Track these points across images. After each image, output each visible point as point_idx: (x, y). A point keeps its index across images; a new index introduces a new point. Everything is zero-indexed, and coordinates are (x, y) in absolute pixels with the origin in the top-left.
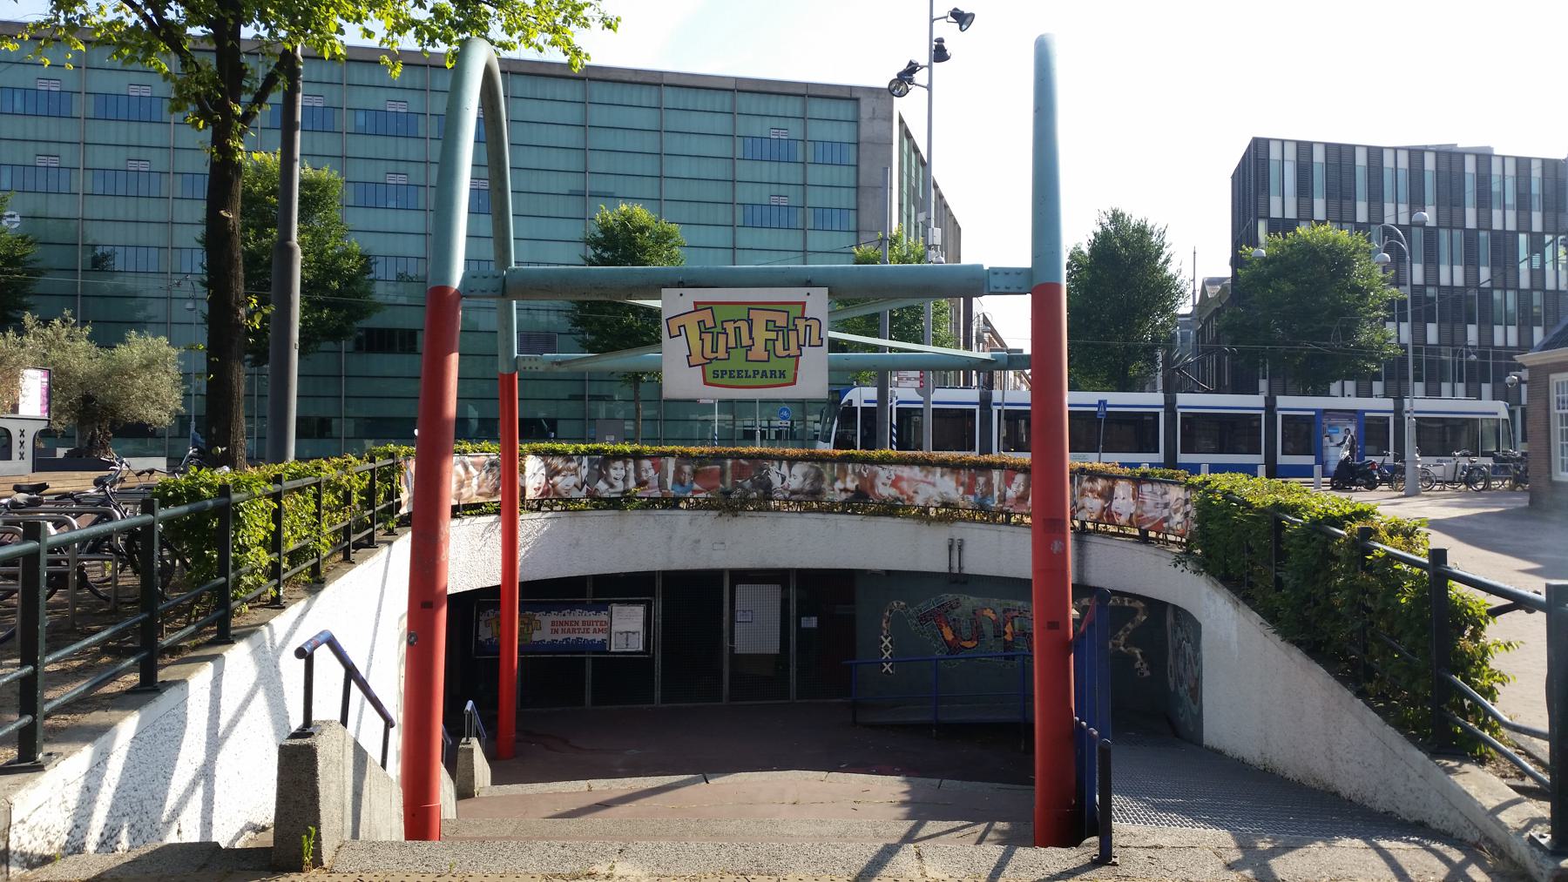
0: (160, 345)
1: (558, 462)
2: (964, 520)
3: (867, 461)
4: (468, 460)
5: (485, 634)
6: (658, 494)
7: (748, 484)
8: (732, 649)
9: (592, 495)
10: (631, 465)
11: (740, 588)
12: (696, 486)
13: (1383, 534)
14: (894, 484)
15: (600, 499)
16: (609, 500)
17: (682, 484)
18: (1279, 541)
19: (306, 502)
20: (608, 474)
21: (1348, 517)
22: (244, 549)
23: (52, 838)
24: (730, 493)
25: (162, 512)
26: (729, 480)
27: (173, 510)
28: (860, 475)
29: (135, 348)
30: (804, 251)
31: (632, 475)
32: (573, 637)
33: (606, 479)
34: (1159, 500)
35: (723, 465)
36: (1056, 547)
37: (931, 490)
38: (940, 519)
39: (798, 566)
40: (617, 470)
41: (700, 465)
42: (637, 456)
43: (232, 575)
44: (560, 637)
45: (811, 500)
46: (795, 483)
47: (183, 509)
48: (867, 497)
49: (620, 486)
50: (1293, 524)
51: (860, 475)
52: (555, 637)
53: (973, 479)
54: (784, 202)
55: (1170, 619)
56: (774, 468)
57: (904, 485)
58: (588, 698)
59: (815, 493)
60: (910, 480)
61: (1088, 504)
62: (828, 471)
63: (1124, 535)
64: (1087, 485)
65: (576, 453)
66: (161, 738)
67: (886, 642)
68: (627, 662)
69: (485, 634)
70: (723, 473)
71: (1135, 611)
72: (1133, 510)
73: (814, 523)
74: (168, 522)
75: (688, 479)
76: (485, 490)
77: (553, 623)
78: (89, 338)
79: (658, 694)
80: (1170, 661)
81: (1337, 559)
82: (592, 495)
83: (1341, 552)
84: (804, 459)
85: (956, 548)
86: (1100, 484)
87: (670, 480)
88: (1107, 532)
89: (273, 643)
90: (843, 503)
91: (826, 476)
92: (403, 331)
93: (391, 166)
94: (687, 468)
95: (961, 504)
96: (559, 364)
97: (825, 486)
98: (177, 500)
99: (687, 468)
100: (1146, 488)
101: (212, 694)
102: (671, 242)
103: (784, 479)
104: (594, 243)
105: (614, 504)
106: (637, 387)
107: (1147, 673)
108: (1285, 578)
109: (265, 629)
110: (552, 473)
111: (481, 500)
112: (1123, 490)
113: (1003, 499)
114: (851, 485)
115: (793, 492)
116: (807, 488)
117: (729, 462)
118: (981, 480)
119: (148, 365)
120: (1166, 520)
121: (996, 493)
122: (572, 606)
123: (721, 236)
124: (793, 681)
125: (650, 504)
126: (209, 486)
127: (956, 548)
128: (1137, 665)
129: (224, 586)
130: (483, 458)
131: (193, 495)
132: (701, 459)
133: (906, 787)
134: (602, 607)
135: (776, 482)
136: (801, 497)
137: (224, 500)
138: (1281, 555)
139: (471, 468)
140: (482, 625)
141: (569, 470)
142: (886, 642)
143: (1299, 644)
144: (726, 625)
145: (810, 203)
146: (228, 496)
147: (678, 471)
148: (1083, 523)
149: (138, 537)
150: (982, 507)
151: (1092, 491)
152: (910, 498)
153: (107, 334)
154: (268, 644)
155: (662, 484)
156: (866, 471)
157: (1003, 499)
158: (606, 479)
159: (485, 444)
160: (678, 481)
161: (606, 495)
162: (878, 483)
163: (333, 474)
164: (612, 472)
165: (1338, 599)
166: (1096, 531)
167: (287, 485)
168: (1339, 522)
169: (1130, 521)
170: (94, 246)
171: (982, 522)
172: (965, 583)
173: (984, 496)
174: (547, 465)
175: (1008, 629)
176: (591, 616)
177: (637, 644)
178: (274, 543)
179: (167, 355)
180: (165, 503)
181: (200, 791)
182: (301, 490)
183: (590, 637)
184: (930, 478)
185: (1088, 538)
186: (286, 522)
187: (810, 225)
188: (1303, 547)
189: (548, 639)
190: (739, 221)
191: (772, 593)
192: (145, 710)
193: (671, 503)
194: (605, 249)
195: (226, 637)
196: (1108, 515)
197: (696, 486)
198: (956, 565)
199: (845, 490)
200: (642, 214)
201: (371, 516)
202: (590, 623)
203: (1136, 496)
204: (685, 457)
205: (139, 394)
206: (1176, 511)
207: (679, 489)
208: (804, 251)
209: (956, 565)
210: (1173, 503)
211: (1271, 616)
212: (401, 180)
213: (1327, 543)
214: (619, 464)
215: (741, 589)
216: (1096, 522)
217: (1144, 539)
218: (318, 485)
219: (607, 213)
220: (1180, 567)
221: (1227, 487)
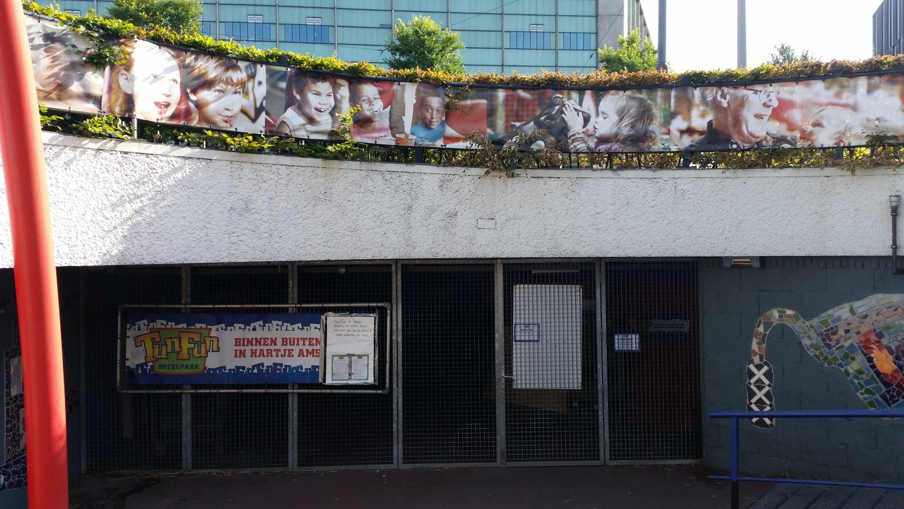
1: (209, 67)
6: (388, 139)
8: (509, 382)
11: (519, 290)
12: (450, 131)
14: (777, 115)
17: (427, 125)
20: (304, 99)
26: (500, 123)
28: (716, 106)
30: (556, 66)
32: (268, 362)
33: (301, 108)
35: (491, 99)
37: (848, 117)
38: (874, 163)
41: (457, 96)
44: (248, 362)
46: (605, 125)
49: (325, 123)
51: (716, 106)
52: (241, 362)
54: (540, 29)
56: (571, 101)
57: (796, 115)
58: (293, 454)
60: (806, 106)
67: (759, 374)
68: (350, 400)
70: (491, 112)
73: (636, 185)
75: (437, 119)
77: (238, 342)
79: (398, 449)
84: (620, 86)
91: (658, 112)
93: (251, 10)
94: (435, 102)
97: (655, 127)
102: (454, 45)
103: (587, 120)
104: (394, 49)
110: (195, 83)
115: (602, 140)
116: (625, 131)
122: (266, 316)
123: (493, 57)
124: (604, 433)
135: (575, 124)
140: (130, 342)
141: (229, 82)
142: (759, 374)
144: (499, 345)
145: (560, 29)
147: (421, 105)
152: (806, 136)
155: (395, 126)
156: (726, 97)
160: (422, 121)
161: (301, 134)
162: (748, 115)
164: (311, 97)
174: (183, 66)
176: (295, 331)
177: (365, 374)
183: (293, 362)
184: (847, 98)
187: (560, 46)
189: (231, 363)
190: (506, 45)
191: (569, 298)
193: (418, 155)
194: (402, 54)
197: (450, 131)
199: (690, 131)
200: (430, 23)
202: (293, 342)
207: (422, 133)
208: (556, 66)
212: (258, 20)
214: (324, 87)
219: (405, 25)
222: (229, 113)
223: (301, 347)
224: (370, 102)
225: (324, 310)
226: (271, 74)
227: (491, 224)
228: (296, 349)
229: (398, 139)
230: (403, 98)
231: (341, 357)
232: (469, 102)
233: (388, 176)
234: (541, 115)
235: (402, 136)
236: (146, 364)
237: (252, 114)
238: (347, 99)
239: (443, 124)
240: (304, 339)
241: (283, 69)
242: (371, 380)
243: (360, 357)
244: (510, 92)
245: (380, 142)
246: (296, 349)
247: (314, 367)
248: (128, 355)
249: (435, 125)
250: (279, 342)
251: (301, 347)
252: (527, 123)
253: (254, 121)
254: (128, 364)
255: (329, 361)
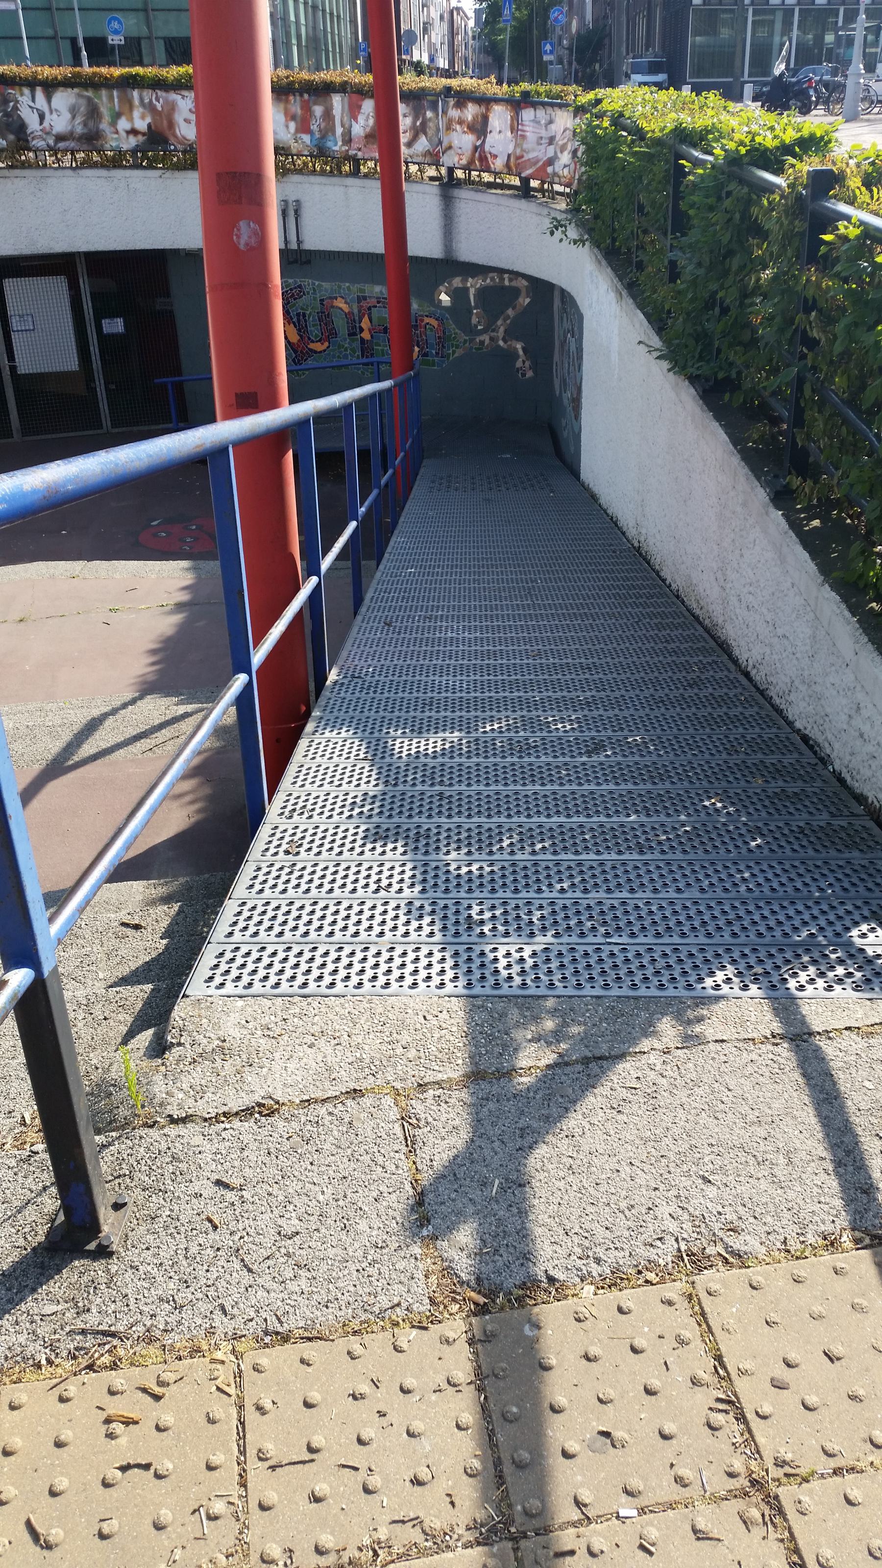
2: (300, 172)
3: (158, 84)
8: (13, 369)
13: (854, 183)
18: (677, 196)
21: (787, 149)
34: (544, 133)
36: (244, 233)
39: (84, 248)
45: (88, 148)
46: (60, 123)
48: (166, 141)
50: (703, 162)
51: (151, 108)
53: (307, 108)
55: (557, 303)
56: (24, 98)
59: (91, 139)
61: (456, 143)
62: (106, 101)
63: (502, 186)
64: (454, 113)
71: (516, 292)
72: (510, 149)
80: (556, 357)
81: (761, 233)
83: (771, 224)
85: (291, 213)
86: (471, 111)
88: (481, 183)
90: (134, 152)
91: (104, 110)
95: (295, 147)
97: (104, 126)
100: (528, 114)
103: (42, 117)
107: (530, 374)
108: (681, 263)
112: (499, 117)
113: (348, 139)
114: (141, 125)
115: (60, 138)
116: (79, 130)
118: (318, 110)
120: (550, 162)
121: (339, 130)
127: (291, 213)
128: (519, 364)
133: (188, 579)
136: (72, 144)
138: (680, 223)
143: (693, 380)
148: (451, 170)
150: (321, 152)
151: (461, 122)
156: (160, 99)
157: (348, 139)
165: (761, 310)
166: (468, 181)
168: (771, 159)
169: (507, 165)
171: (323, 173)
172: (308, 262)
173: (323, 137)
175: (365, 323)
185: (457, 192)
188: (711, 209)
191: (55, 288)
196: (480, 158)
198: (293, 237)
199: (133, 132)
203: (515, 127)
206: (563, 149)
209: (293, 237)
210: (553, 134)
211: (658, 320)
213: (749, 203)
216: (467, 168)
217: (525, 192)
220: (558, 234)
221: (617, 106)
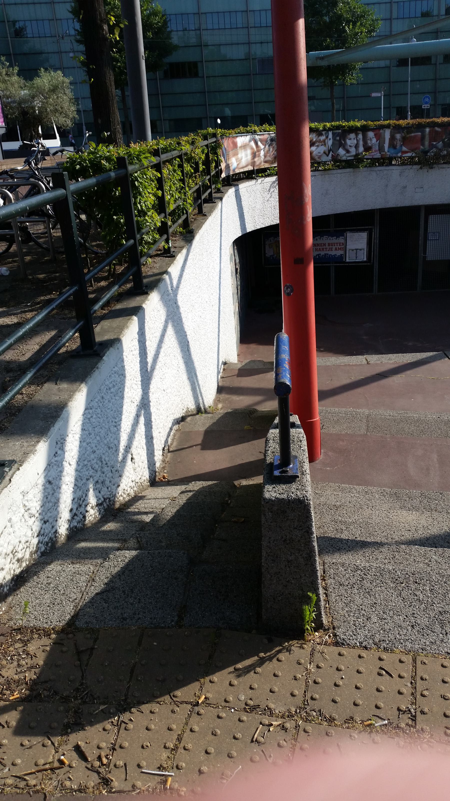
0: (59, 76)
4: (257, 137)
5: (269, 252)
6: (378, 155)
7: (440, 144)
8: (425, 258)
9: (335, 159)
10: (360, 136)
12: (404, 149)
15: (341, 161)
16: (346, 161)
19: (175, 171)
20: (346, 143)
22: (142, 213)
23: (20, 555)
24: (428, 152)
25: (73, 186)
26: (427, 143)
27: (82, 183)
29: (45, 80)
31: (361, 143)
32: (322, 253)
35: (423, 133)
40: (351, 140)
41: (408, 133)
42: (365, 129)
43: (138, 236)
47: (92, 181)
49: (353, 151)
65: (324, 129)
66: (107, 397)
68: (356, 267)
69: (269, 252)
70: (423, 138)
74: (80, 193)
75: (399, 144)
76: (268, 158)
78: (19, 75)
82: (335, 159)
87: (386, 146)
89: (172, 287)
92: (190, 63)
94: (398, 136)
96: (322, 58)
98: (84, 173)
99: (398, 136)
101: (139, 341)
105: (353, 164)
106: (332, 89)
109: (166, 277)
111: (267, 166)
117: (427, 130)
119: (54, 89)
125: (374, 162)
126: (108, 159)
129: (134, 247)
130: (266, 136)
131: (96, 167)
132: (409, 129)
134: (340, 233)
137: (122, 171)
139: (259, 143)
140: (267, 247)
141: (320, 141)
146: (125, 168)
147: (392, 138)
149: (60, 204)
153: (29, 74)
154: (170, 289)
155: (381, 149)
158: (344, 146)
159: (266, 126)
160: (392, 145)
161: (344, 158)
163: (187, 148)
164: (349, 142)
167: (164, 157)
170: (14, 22)
176: (334, 240)
177: (363, 257)
178: (160, 205)
179: (63, 82)
180: (74, 175)
181: (142, 420)
182: (170, 161)
183: (333, 253)
186: (166, 188)
192: (91, 381)
193: (385, 161)
195: (142, 288)
197: (404, 149)
201: (209, 180)
202: (332, 244)
204: (397, 128)
205: (52, 108)
207: (392, 151)
214: (352, 136)
215: (432, 218)
218: (180, 157)
222: (319, 154)
223: (336, 246)
224: (371, 140)
225: (345, 231)
226: (333, 134)
227: (421, 190)
228: (334, 247)
229: (382, 155)
230: (384, 136)
231: (353, 250)
232: (413, 134)
233: (378, 172)
234: (445, 139)
235: (384, 153)
236: (274, 255)
237: (327, 153)
238: (361, 139)
239: (401, 146)
240: (337, 243)
241: (338, 131)
242: (365, 259)
243: (360, 250)
244: (432, 129)
245: (375, 157)
246: (334, 248)
247: (341, 255)
248: (266, 252)
249: (398, 147)
250: (327, 245)
251: (336, 246)
252: (439, 142)
253: (328, 156)
254: (267, 255)
255: (347, 252)
